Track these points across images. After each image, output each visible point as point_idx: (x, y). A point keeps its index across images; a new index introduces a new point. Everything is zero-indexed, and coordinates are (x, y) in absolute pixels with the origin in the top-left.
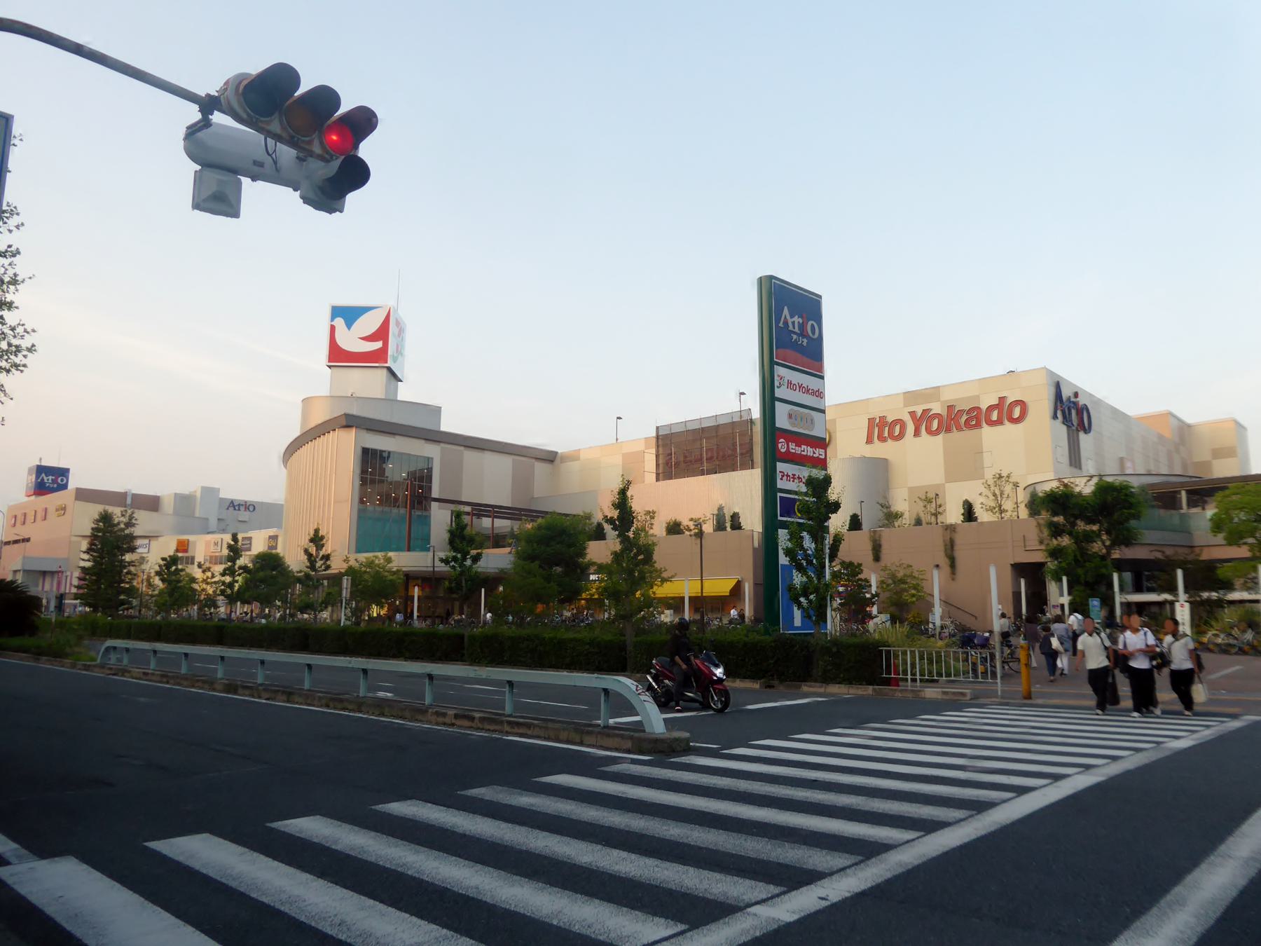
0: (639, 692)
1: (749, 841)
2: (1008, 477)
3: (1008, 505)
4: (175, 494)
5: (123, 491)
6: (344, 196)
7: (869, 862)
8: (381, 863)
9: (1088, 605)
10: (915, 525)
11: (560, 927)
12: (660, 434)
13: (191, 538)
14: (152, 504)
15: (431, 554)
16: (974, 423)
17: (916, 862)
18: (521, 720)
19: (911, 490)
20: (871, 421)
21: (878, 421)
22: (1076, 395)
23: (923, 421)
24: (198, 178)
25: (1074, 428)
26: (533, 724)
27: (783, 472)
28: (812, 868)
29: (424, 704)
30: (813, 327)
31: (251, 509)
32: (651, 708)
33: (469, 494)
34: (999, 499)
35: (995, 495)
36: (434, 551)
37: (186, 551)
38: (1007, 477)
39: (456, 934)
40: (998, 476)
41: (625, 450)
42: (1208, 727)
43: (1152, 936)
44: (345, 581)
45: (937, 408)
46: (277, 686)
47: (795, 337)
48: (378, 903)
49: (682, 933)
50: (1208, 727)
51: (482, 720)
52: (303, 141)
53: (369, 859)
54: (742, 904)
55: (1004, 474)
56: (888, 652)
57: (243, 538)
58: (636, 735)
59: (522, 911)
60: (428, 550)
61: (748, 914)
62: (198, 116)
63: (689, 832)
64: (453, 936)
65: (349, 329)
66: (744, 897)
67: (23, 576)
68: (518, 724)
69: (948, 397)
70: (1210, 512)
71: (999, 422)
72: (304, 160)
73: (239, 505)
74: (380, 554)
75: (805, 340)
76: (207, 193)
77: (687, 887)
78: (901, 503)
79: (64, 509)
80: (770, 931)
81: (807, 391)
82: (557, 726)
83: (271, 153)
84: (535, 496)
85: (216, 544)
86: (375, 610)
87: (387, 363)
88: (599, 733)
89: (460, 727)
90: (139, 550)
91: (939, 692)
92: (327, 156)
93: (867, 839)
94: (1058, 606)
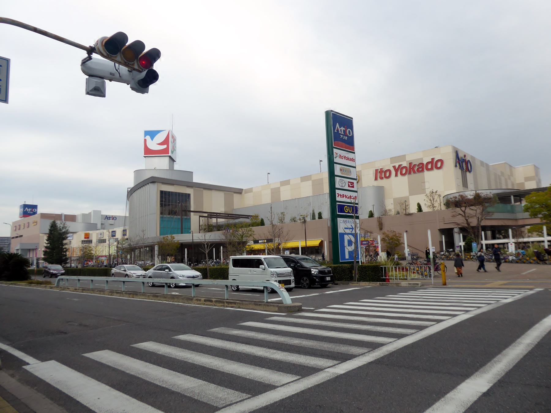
0: (280, 287)
1: (326, 344)
2: (436, 192)
3: (436, 204)
4: (83, 214)
5: (60, 214)
6: (148, 86)
7: (375, 351)
8: (177, 358)
9: (472, 245)
10: (369, 217)
11: (250, 379)
13: (90, 232)
14: (72, 218)
15: (191, 234)
17: (394, 350)
18: (232, 301)
19: (395, 199)
20: (376, 170)
22: (465, 156)
23: (399, 170)
24: (88, 81)
25: (464, 170)
26: (237, 302)
27: (338, 194)
28: (351, 354)
29: (192, 296)
32: (285, 294)
33: (207, 208)
34: (432, 202)
35: (430, 200)
36: (192, 233)
37: (88, 238)
38: (436, 192)
39: (209, 383)
40: (432, 192)
41: (272, 187)
42: (520, 294)
43: (486, 374)
44: (156, 247)
45: (405, 164)
46: (130, 292)
47: (342, 136)
48: (177, 373)
49: (299, 379)
50: (520, 294)
51: (216, 301)
52: (130, 64)
53: (173, 357)
54: (323, 368)
55: (434, 191)
56: (385, 268)
57: (112, 231)
58: (280, 305)
59: (234, 374)
60: (190, 233)
61: (325, 372)
62: (87, 55)
63: (301, 342)
64: (207, 384)
65: (152, 140)
66: (324, 365)
67: (21, 251)
68: (231, 303)
69: (409, 158)
70: (524, 203)
71: (432, 169)
72: (131, 72)
73: (110, 217)
74: (169, 236)
75: (346, 137)
76: (92, 87)
77: (301, 362)
78: (390, 206)
79: (36, 222)
80: (334, 377)
81: (348, 159)
82: (247, 303)
83: (117, 70)
84: (234, 208)
85: (101, 234)
86: (169, 259)
87: (169, 154)
88: (264, 305)
89: (206, 305)
90: (68, 238)
91: (407, 284)
92: (140, 69)
93: (374, 342)
94: (459, 246)
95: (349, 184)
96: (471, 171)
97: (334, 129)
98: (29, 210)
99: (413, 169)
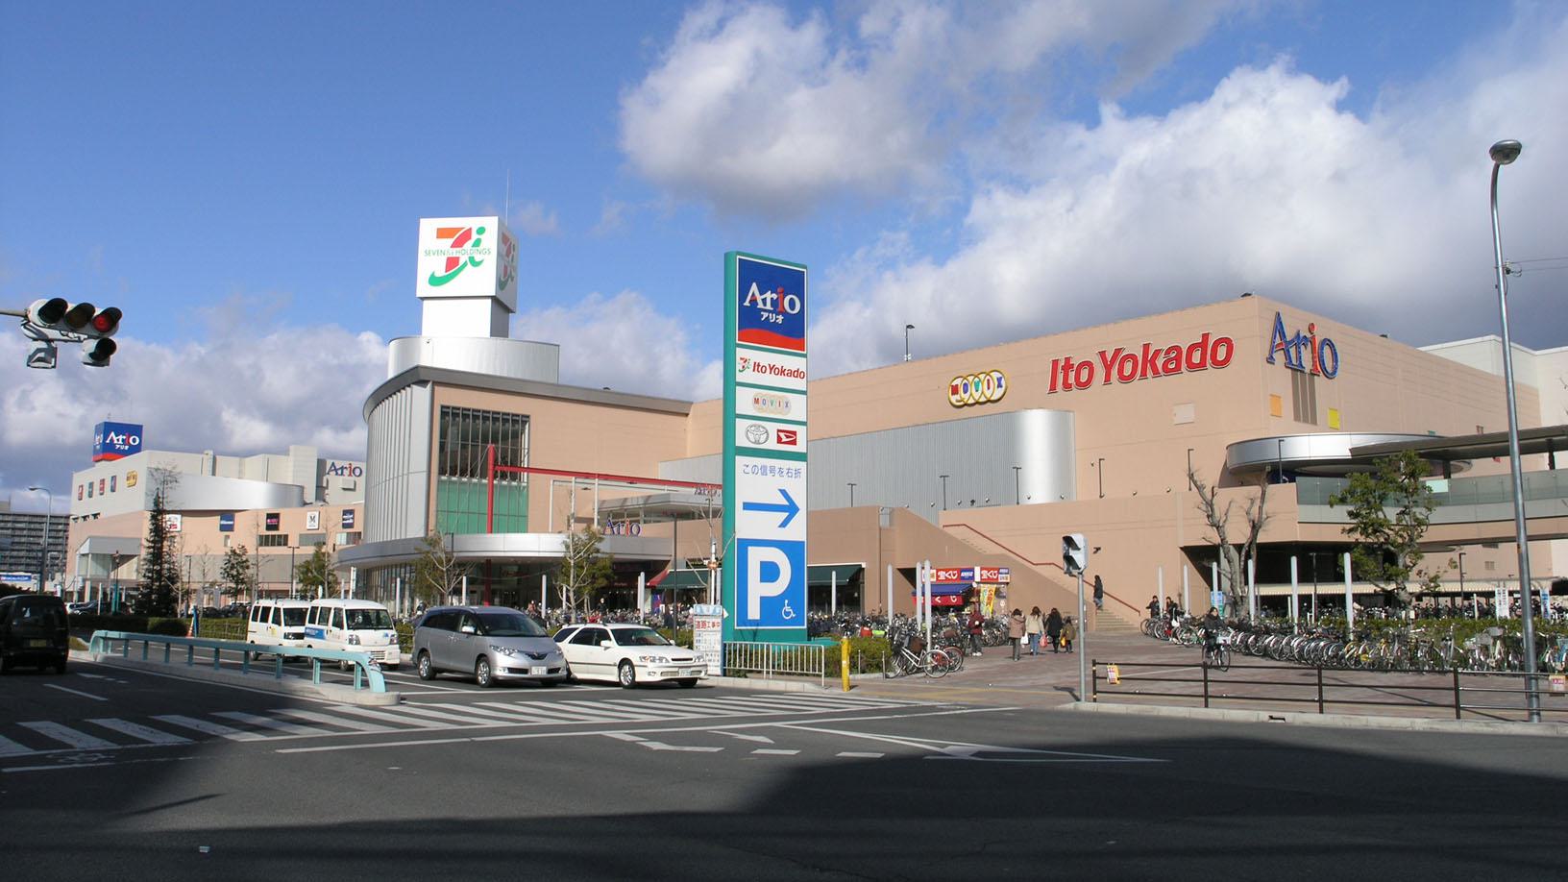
16: (1173, 366)
20: (1055, 363)
30: (792, 301)
37: (275, 527)
71: (1202, 365)
75: (781, 317)
79: (134, 477)
95: (779, 436)
96: (1334, 372)
97: (742, 299)
99: (1153, 362)
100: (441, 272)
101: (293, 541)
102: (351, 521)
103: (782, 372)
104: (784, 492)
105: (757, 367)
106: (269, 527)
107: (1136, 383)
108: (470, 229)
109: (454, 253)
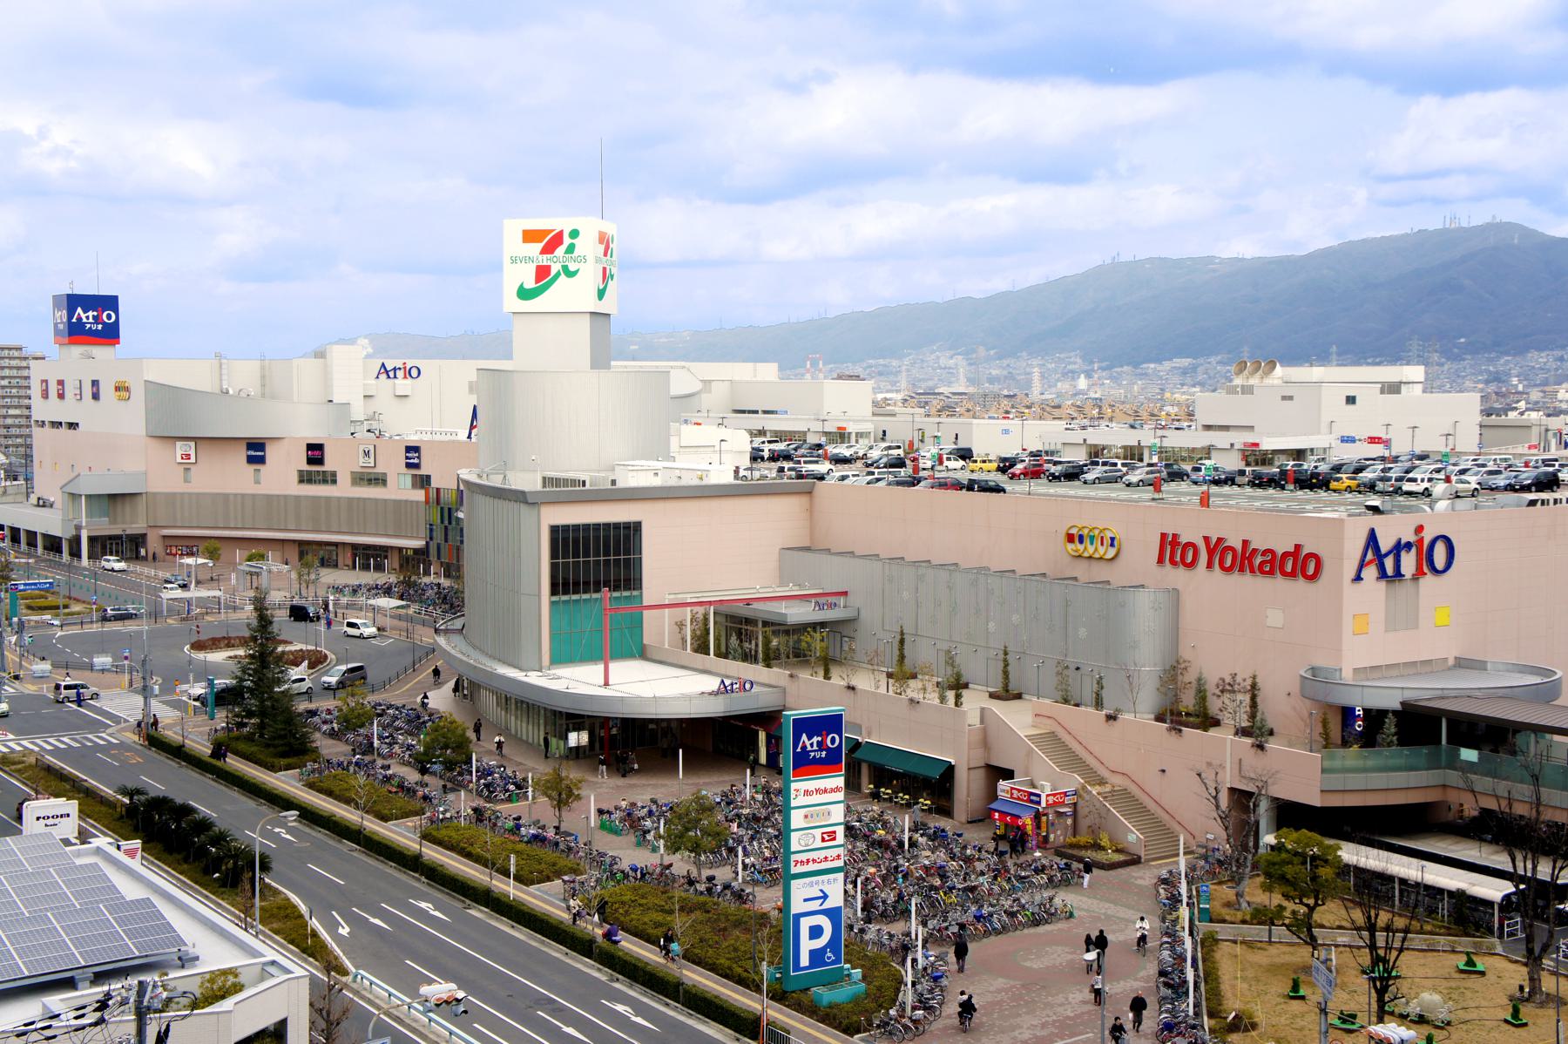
12: (645, 612)
20: (1164, 536)
21: (1170, 539)
31: (414, 373)
37: (320, 461)
71: (1293, 574)
97: (795, 747)
98: (86, 317)
100: (530, 283)
101: (344, 479)
102: (416, 461)
103: (825, 791)
104: (821, 891)
105: (807, 793)
106: (310, 461)
107: (1235, 577)
108: (560, 234)
109: (544, 260)
